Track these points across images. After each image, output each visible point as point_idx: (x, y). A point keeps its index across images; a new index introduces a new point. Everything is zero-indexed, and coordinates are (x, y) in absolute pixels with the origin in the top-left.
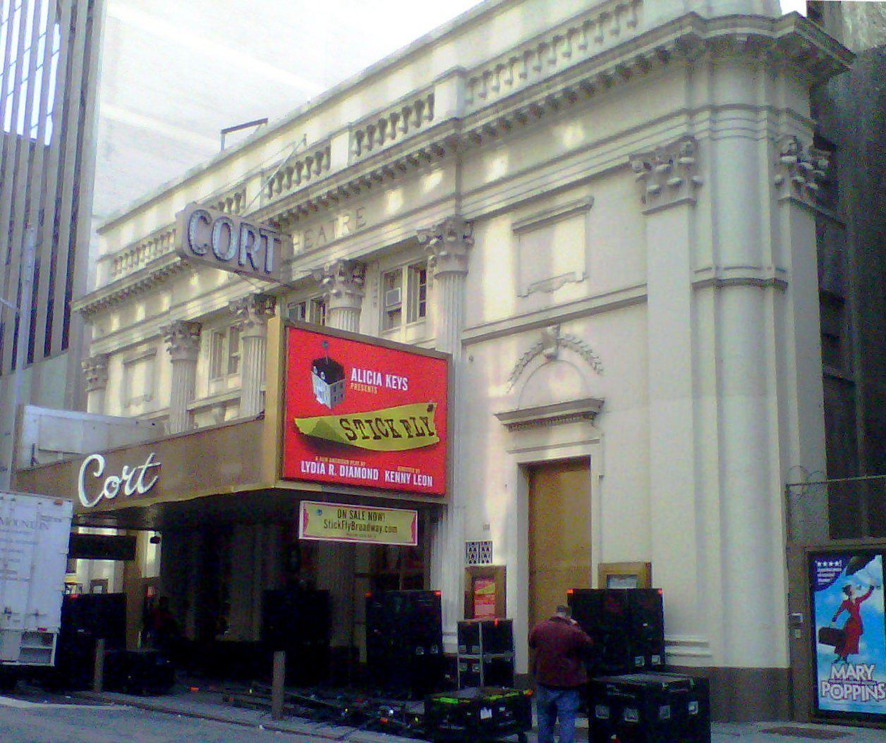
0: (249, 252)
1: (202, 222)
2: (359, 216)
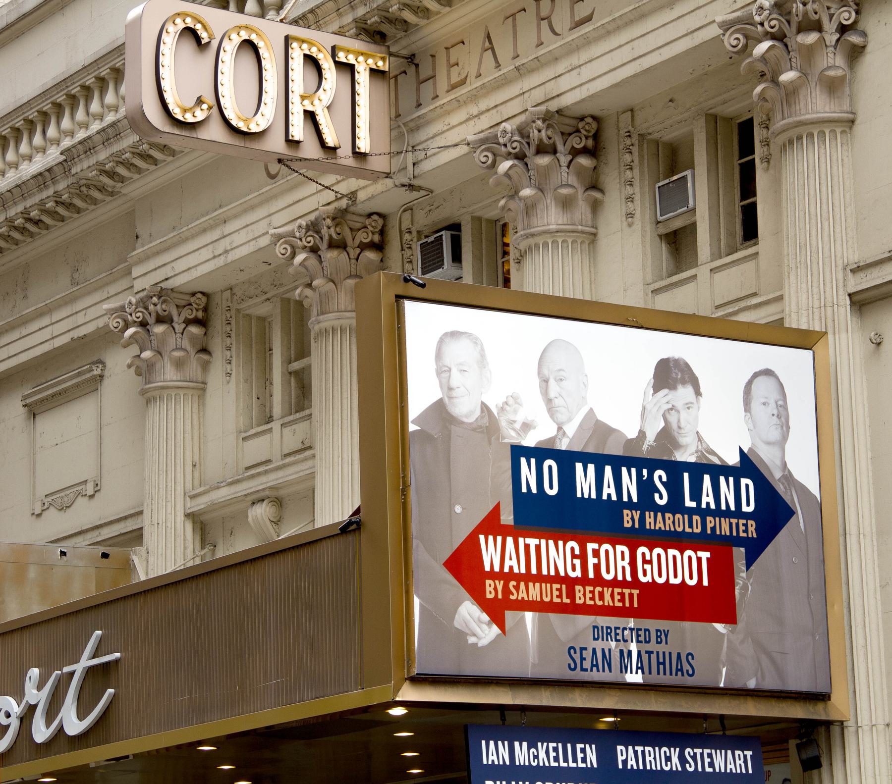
0: (310, 108)
1: (189, 45)
2: (452, 61)
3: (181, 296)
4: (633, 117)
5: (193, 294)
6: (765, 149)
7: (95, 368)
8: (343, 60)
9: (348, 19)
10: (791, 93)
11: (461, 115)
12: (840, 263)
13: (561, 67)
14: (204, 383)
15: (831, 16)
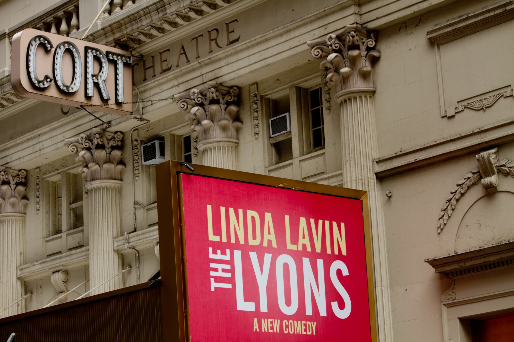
0: (96, 81)
1: (41, 52)
3: (15, 171)
4: (257, 87)
5: (20, 170)
6: (328, 104)
8: (111, 58)
9: (111, 39)
10: (345, 79)
11: (169, 85)
12: (371, 158)
13: (222, 63)
14: (25, 214)
15: (363, 43)
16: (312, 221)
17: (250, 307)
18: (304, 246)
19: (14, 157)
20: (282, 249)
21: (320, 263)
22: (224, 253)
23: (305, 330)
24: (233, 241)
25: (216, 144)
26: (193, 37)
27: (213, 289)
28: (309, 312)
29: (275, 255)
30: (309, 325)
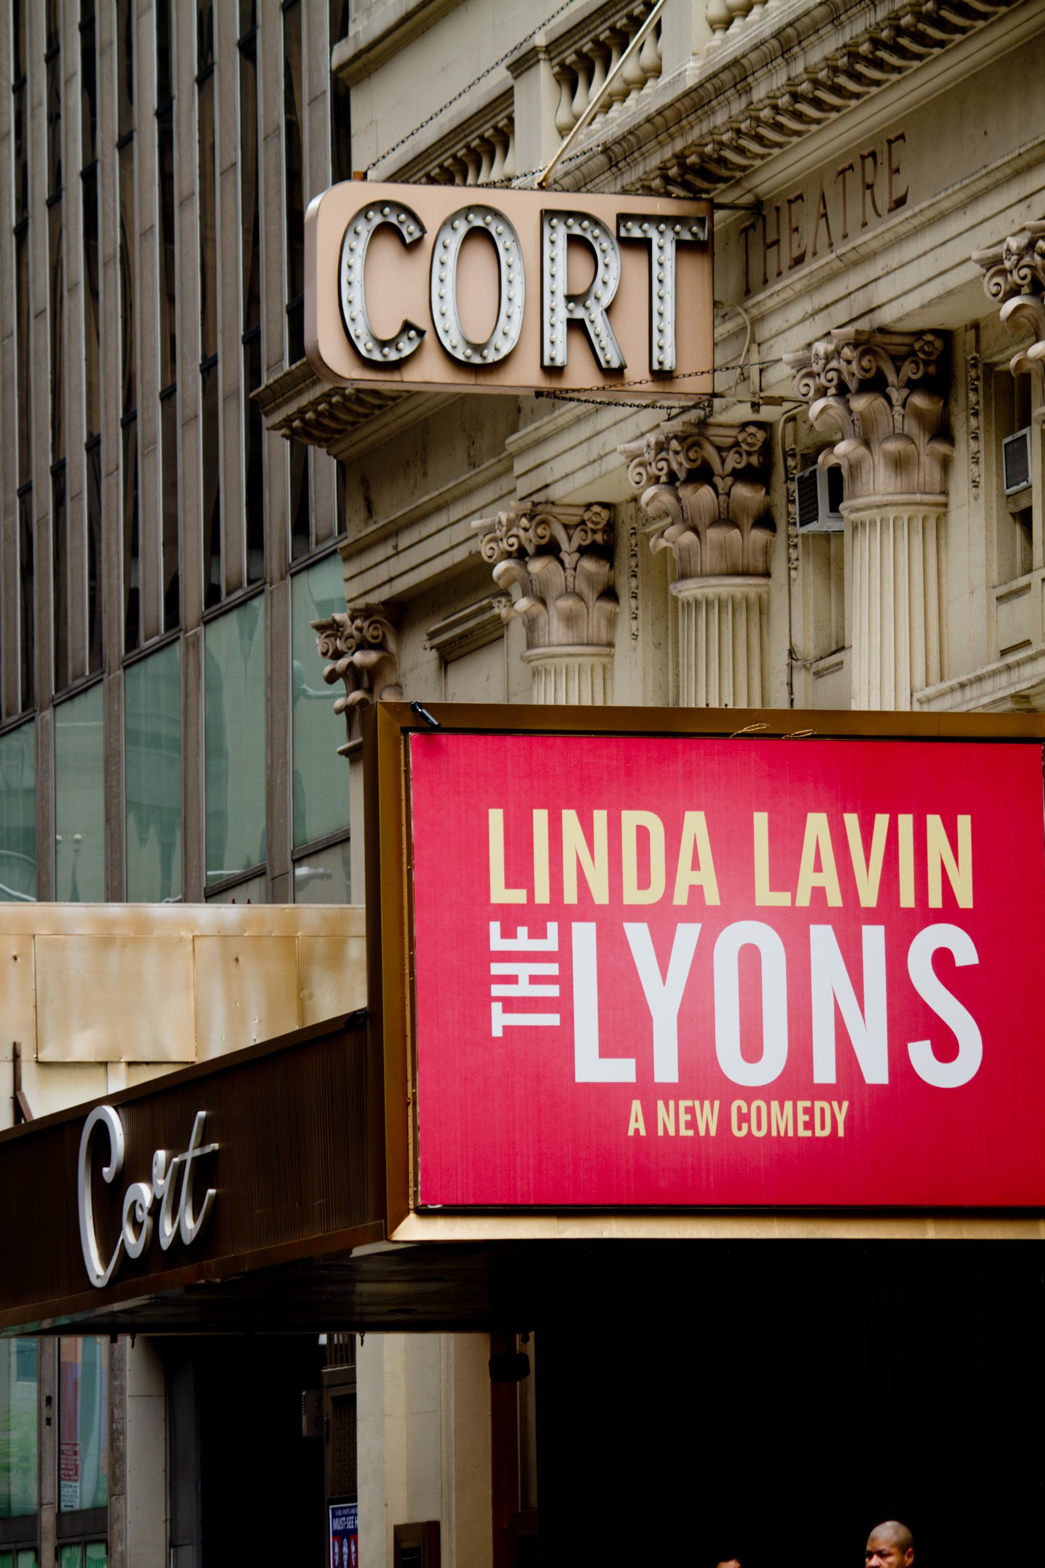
3: (571, 511)
5: (588, 506)
7: (495, 604)
13: (876, 268)
14: (611, 645)
16: (852, 821)
17: (622, 1071)
18: (819, 893)
19: (559, 467)
20: (738, 903)
21: (874, 939)
22: (538, 932)
23: (809, 1125)
24: (570, 896)
25: (875, 511)
26: (840, 168)
27: (497, 1032)
28: (825, 1072)
29: (712, 923)
30: (822, 1110)
